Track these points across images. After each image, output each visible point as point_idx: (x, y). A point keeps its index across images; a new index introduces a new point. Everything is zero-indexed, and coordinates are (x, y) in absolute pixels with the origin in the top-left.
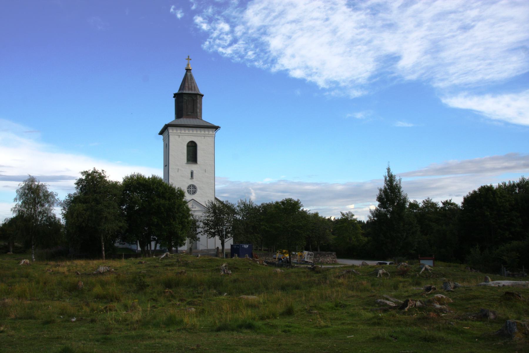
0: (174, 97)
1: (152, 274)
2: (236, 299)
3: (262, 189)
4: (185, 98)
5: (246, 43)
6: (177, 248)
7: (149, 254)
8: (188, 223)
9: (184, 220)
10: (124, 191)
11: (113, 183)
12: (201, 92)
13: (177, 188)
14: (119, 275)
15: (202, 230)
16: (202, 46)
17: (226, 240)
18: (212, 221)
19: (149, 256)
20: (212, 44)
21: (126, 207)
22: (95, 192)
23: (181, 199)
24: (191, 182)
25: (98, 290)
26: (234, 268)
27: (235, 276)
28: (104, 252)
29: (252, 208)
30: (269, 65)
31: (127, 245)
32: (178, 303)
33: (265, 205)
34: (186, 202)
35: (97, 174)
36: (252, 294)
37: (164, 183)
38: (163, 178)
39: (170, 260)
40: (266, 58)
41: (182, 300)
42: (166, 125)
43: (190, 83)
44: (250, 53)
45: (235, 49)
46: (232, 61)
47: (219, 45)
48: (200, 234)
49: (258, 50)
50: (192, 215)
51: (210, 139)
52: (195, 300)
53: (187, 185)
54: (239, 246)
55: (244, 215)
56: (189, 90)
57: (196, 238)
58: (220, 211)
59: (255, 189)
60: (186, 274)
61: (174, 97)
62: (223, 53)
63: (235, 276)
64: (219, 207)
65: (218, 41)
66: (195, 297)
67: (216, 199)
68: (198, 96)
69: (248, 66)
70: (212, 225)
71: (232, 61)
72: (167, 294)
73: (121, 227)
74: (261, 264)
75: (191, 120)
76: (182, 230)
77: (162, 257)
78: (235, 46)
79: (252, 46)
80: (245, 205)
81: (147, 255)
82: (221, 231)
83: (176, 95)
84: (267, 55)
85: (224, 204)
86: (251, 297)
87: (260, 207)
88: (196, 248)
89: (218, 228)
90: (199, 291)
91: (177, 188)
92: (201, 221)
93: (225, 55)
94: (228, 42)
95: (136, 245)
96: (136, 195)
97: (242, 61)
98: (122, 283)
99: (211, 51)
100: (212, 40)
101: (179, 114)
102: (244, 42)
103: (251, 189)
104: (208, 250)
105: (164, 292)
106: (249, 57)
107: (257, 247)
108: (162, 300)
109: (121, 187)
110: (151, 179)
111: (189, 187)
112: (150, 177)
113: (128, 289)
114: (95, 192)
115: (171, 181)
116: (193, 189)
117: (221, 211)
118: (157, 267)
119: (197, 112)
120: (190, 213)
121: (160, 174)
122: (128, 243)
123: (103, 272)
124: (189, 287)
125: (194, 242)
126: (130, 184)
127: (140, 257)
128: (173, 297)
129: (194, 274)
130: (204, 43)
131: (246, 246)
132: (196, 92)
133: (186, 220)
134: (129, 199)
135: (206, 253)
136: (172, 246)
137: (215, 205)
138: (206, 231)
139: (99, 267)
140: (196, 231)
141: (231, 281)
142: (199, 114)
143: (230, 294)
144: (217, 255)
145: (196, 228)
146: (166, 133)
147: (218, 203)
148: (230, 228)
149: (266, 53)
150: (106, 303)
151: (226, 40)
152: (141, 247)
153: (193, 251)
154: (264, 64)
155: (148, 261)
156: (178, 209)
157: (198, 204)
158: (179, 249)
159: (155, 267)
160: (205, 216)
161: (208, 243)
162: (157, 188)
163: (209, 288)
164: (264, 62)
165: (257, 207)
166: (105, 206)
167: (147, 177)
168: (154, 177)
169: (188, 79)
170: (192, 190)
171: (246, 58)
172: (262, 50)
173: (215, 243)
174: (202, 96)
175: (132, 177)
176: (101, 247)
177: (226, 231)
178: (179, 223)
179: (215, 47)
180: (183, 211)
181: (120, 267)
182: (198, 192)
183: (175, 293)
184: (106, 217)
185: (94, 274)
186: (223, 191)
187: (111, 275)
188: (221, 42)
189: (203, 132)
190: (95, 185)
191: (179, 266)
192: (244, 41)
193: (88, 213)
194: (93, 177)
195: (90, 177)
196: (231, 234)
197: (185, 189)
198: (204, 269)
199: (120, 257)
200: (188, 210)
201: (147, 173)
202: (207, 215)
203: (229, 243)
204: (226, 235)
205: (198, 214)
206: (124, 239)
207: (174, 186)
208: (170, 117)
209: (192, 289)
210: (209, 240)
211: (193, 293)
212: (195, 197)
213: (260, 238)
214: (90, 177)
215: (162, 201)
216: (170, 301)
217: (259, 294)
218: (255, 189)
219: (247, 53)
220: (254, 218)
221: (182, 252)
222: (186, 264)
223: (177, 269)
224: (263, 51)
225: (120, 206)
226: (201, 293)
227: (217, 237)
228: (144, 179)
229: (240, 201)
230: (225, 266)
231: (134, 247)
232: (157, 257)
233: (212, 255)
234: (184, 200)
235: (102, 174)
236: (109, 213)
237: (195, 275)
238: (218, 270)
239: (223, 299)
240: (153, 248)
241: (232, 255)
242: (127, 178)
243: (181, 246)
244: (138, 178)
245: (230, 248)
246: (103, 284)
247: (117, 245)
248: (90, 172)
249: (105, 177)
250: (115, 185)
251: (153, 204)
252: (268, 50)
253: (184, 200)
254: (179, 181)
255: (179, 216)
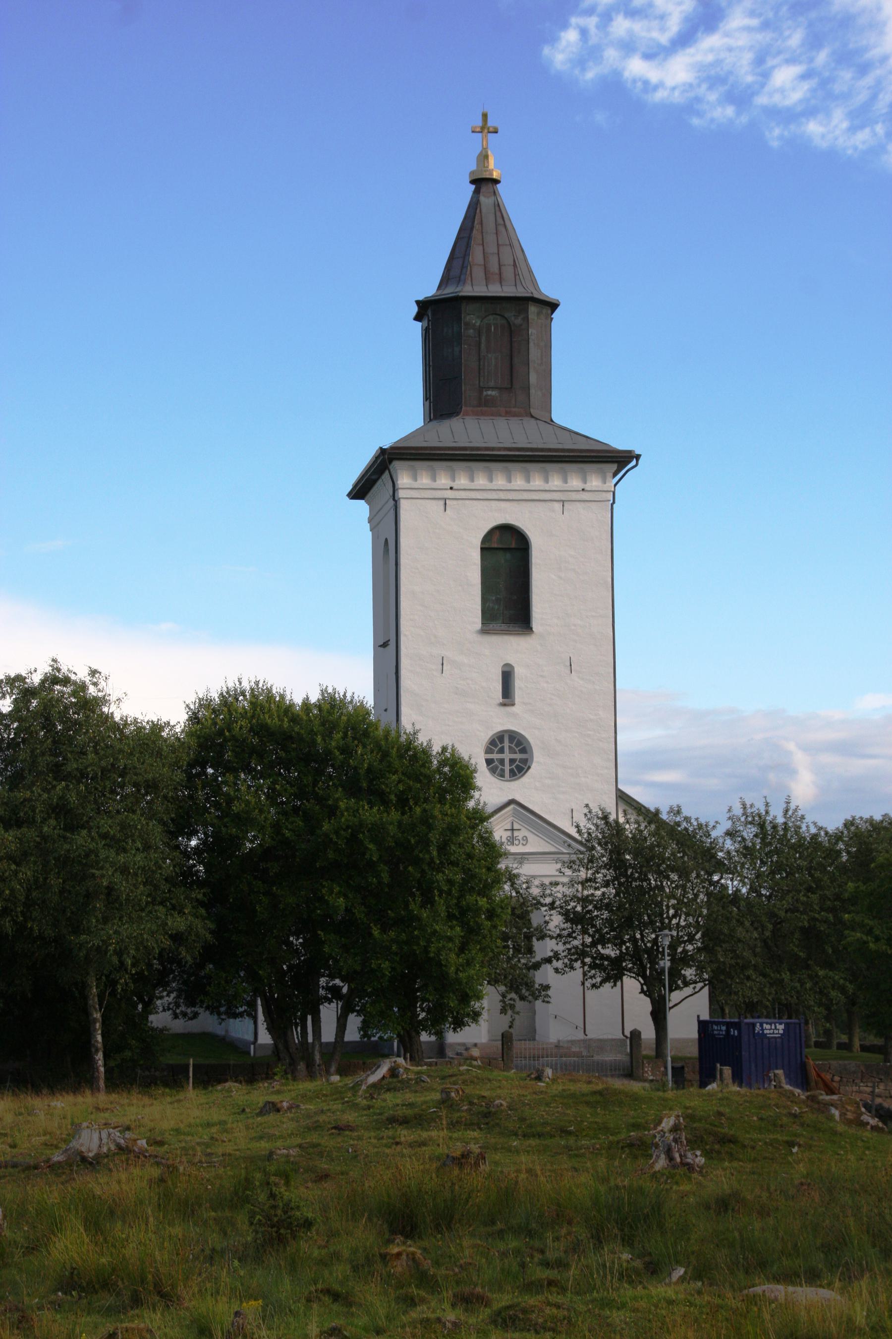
0: (418, 318)
1: (323, 1165)
2: (732, 1301)
3: (846, 748)
4: (472, 318)
5: (766, 25)
6: (440, 1034)
7: (310, 1065)
8: (491, 914)
9: (471, 898)
10: (191, 765)
11: (140, 729)
12: (548, 289)
13: (436, 749)
14: (172, 1169)
15: (560, 948)
16: (546, 51)
17: (676, 996)
18: (608, 907)
19: (311, 1075)
20: (593, 40)
21: (204, 842)
22: (57, 771)
23: (458, 803)
24: (502, 721)
25: (71, 1246)
26: (716, 1140)
27: (722, 1178)
28: (100, 1057)
29: (800, 845)
30: (880, 129)
31: (206, 1022)
32: (451, 1316)
33: (864, 827)
34: (479, 817)
35: (68, 690)
36: (813, 1277)
37: (375, 726)
38: (370, 702)
39: (410, 1097)
40: (862, 97)
41: (467, 1301)
42: (382, 451)
43: (492, 249)
44: (784, 76)
45: (710, 58)
46: (695, 121)
47: (628, 47)
48: (548, 969)
49: (822, 57)
50: (512, 878)
51: (590, 516)
52: (531, 1300)
53: (485, 736)
54: (737, 1026)
55: (759, 876)
56: (488, 280)
57: (529, 985)
58: (642, 858)
59: (808, 749)
60: (485, 1168)
61: (418, 318)
62: (646, 83)
63: (722, 1178)
64: (638, 838)
65: (621, 26)
66: (531, 1287)
67: (622, 797)
68: (533, 309)
69: (775, 144)
70: (609, 921)
71: (695, 121)
72: (399, 1267)
73: (177, 938)
74: (849, 1123)
75: (501, 423)
76: (462, 949)
77: (374, 1078)
78: (710, 45)
79: (796, 39)
80: (762, 826)
81: (302, 1066)
82: (648, 951)
83: (425, 309)
84: (869, 80)
85: (661, 824)
86: (805, 1295)
87: (838, 837)
88: (531, 1034)
89: (633, 940)
90: (551, 1255)
91: (436, 749)
92: (552, 906)
93: (660, 95)
94: (674, 25)
95: (248, 1022)
96: (248, 789)
97: (744, 119)
98: (187, 1209)
99: (590, 75)
100: (592, 22)
101: (444, 392)
102: (755, 22)
103: (791, 746)
104: (587, 1043)
105: (384, 1258)
106: (777, 99)
107: (828, 1033)
108: (375, 1299)
109: (177, 745)
110: (319, 706)
111: (496, 742)
112: (313, 699)
113: (214, 1239)
114: (57, 771)
115: (409, 719)
116: (512, 754)
117: (648, 859)
118: (349, 1128)
119: (527, 389)
120: (502, 866)
121: (357, 683)
122: (213, 1009)
123: (98, 1157)
124: (501, 1234)
125: (520, 1005)
126: (221, 733)
127: (269, 1077)
128: (425, 1280)
129: (522, 1166)
130: (553, 40)
131: (774, 1029)
132: (520, 292)
133: (483, 902)
134: (217, 805)
135: (578, 1060)
136: (416, 1027)
137: (618, 829)
138: (580, 953)
139: (76, 1128)
140: (530, 951)
141: (708, 1207)
142: (535, 394)
143: (701, 1272)
144: (630, 1073)
145: (528, 937)
146: (382, 488)
147: (633, 817)
148: (691, 939)
149: (864, 69)
150: (109, 1312)
151: (662, 17)
152: (271, 1029)
153: (518, 1046)
154: (853, 129)
155: (305, 1097)
156: (443, 848)
157: (539, 823)
158: (452, 1037)
159: (339, 1128)
160: (572, 883)
161: (589, 1010)
162: (346, 751)
163: (599, 1239)
164: (851, 115)
165: (822, 837)
166: (105, 836)
167: (298, 700)
168: (332, 698)
169: (482, 226)
170: (507, 756)
171: (762, 100)
172: (846, 57)
173: (624, 1006)
174: (553, 306)
175: (228, 701)
176: (87, 1032)
177: (673, 956)
178: (450, 917)
179: (611, 54)
180: (470, 856)
181: (178, 1131)
182: (535, 768)
183: (437, 1264)
184: (110, 889)
185: (53, 1167)
186: (655, 759)
187: (136, 1171)
188: (638, 27)
189: (555, 481)
190: (58, 742)
191: (453, 1125)
192: (752, 14)
193: (27, 872)
194: (49, 705)
195: (35, 703)
196: (700, 969)
197: (474, 753)
198: (572, 1141)
199: (174, 1079)
200: (493, 851)
201: (300, 678)
202: (583, 874)
203: (689, 1010)
204: (675, 973)
205: (538, 869)
206: (194, 994)
207: (422, 739)
208: (402, 412)
209: (514, 1244)
210: (591, 994)
211: (523, 1265)
212: (522, 790)
213: (843, 990)
214: (35, 703)
215: (370, 814)
216: (411, 1302)
217: (848, 1278)
218: (808, 749)
219: (766, 75)
220: (809, 889)
221: (464, 1055)
222: (487, 1115)
223: (442, 1139)
224: (855, 60)
225: (174, 835)
226: (562, 1265)
227: (631, 984)
228: (285, 709)
229: (738, 811)
230: (675, 1129)
231: (240, 1029)
232: (349, 1081)
233: (602, 1069)
234: (471, 804)
235: (92, 690)
236: (124, 870)
237: (529, 1171)
238: (641, 1148)
239: (670, 1302)
240: (328, 1034)
241: (707, 1076)
242: (205, 704)
243: (458, 1024)
244: (254, 703)
245: (695, 1035)
246: (98, 1218)
247: (159, 1019)
248: (36, 679)
249: (104, 701)
250: (149, 739)
251: (326, 827)
252: (874, 53)
253: (471, 804)
254: (445, 718)
255: (450, 882)
